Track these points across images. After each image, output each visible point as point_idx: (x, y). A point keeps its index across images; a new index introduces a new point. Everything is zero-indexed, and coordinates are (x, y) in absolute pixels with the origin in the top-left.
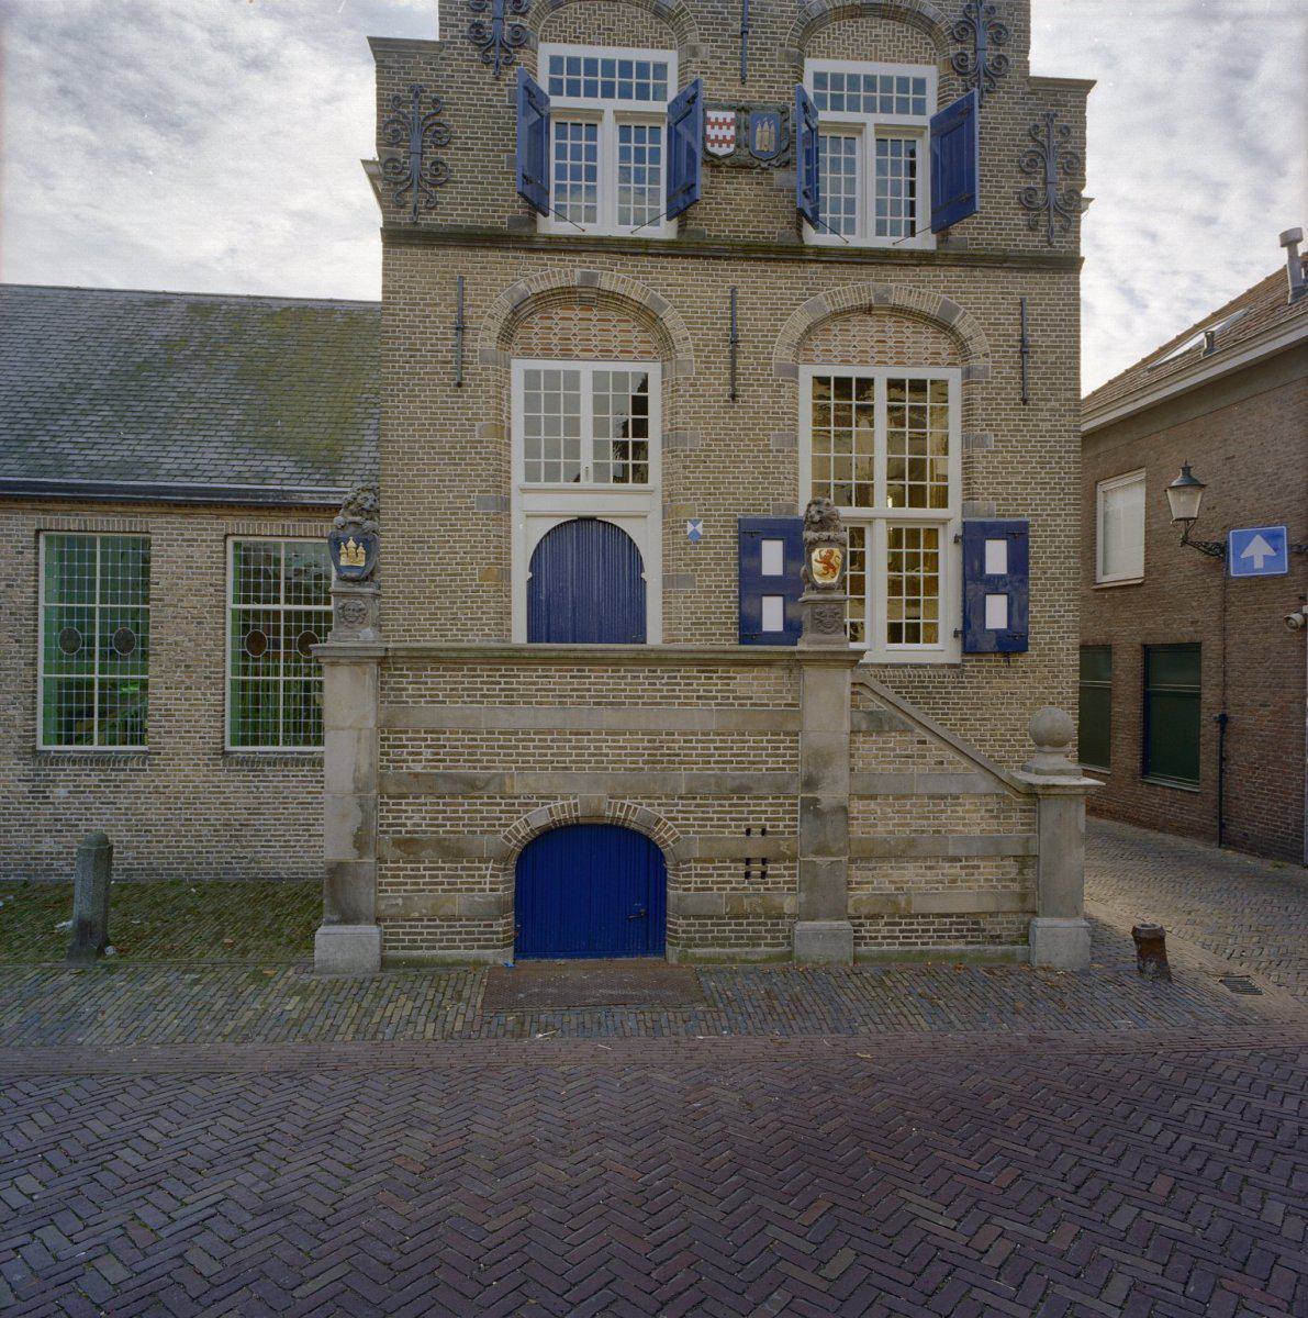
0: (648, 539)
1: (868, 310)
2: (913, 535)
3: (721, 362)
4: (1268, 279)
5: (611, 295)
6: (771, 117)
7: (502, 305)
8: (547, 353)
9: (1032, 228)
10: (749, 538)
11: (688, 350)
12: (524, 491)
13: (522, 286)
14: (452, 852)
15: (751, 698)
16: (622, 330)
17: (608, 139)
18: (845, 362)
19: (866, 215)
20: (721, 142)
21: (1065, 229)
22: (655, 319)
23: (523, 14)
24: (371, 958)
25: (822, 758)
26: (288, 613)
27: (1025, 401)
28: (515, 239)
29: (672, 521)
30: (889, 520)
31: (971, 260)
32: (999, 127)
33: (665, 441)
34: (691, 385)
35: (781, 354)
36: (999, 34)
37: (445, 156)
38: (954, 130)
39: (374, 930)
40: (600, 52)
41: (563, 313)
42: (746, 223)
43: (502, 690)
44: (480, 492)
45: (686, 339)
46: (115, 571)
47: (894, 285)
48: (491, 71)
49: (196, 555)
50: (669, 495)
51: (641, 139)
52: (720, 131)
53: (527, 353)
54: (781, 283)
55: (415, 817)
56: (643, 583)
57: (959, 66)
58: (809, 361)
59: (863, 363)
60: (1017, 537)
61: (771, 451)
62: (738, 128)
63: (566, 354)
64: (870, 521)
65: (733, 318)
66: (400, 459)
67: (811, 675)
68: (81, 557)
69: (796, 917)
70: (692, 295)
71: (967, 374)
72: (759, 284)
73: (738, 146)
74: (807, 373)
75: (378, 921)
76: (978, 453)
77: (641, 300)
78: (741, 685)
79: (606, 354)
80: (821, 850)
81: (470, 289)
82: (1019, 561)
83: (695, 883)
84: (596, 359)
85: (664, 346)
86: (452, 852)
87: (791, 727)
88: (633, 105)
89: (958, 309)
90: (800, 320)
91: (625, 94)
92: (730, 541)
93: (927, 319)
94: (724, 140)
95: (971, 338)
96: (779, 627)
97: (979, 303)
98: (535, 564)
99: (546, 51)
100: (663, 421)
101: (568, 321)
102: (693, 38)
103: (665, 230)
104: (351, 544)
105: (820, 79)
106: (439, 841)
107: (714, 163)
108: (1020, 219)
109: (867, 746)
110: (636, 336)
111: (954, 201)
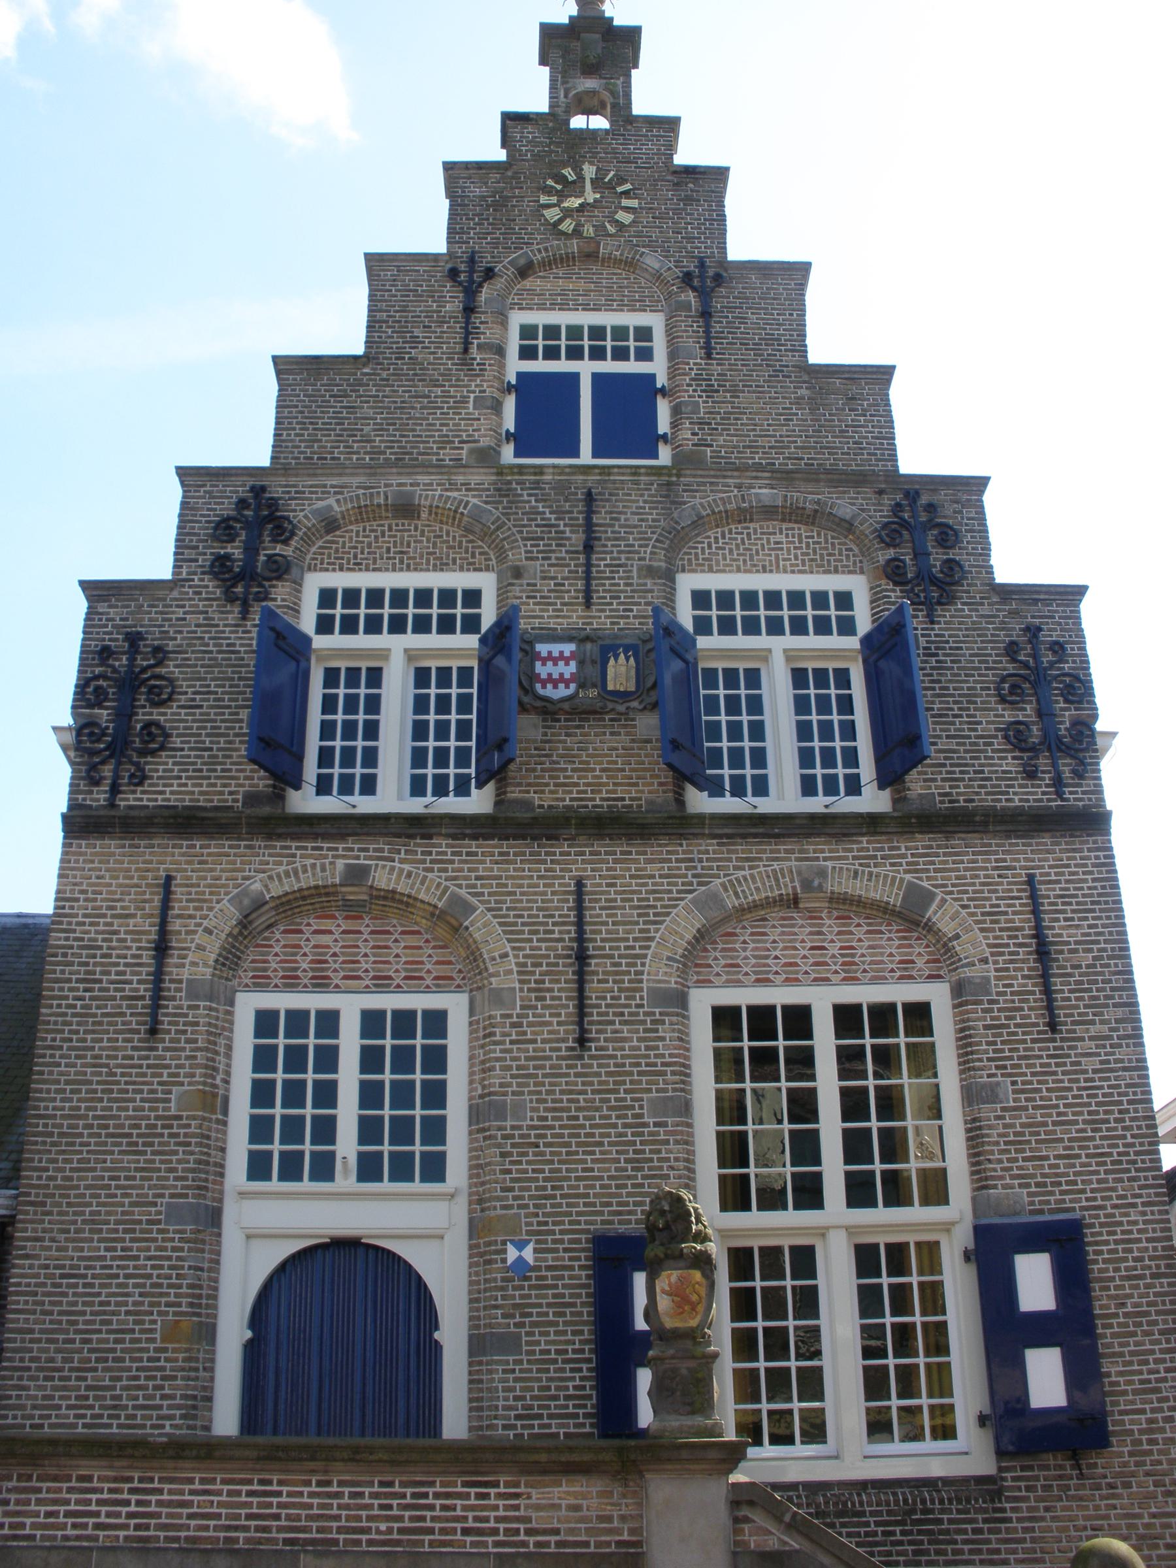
2: (898, 1253)
3: (562, 989)
5: (390, 896)
6: (627, 649)
7: (224, 915)
8: (291, 983)
11: (510, 972)
12: (243, 1195)
13: (257, 886)
15: (556, 1532)
18: (763, 981)
21: (1079, 775)
23: (286, 542)
27: (1053, 1026)
28: (270, 822)
29: (483, 1235)
30: (850, 1230)
32: (959, 640)
33: (476, 1114)
34: (513, 1025)
41: (316, 924)
43: (131, 1515)
44: (172, 1196)
45: (506, 955)
47: (829, 864)
48: (236, 610)
50: (478, 1201)
52: (557, 669)
53: (261, 983)
54: (650, 869)
56: (437, 1347)
57: (894, 572)
58: (705, 983)
59: (791, 981)
60: (1065, 1242)
61: (645, 1125)
62: (581, 663)
63: (321, 983)
64: (822, 1232)
65: (580, 923)
66: (54, 1144)
70: (513, 898)
71: (958, 989)
73: (582, 686)
74: (702, 1003)
76: (987, 1112)
77: (435, 901)
78: (538, 1508)
79: (382, 983)
81: (178, 892)
82: (1072, 1278)
84: (367, 990)
85: (470, 971)
89: (932, 896)
90: (684, 922)
92: (576, 1278)
93: (883, 910)
95: (957, 937)
97: (972, 887)
100: (471, 1082)
101: (326, 936)
105: (700, 599)
108: (1010, 764)
111: (899, 751)
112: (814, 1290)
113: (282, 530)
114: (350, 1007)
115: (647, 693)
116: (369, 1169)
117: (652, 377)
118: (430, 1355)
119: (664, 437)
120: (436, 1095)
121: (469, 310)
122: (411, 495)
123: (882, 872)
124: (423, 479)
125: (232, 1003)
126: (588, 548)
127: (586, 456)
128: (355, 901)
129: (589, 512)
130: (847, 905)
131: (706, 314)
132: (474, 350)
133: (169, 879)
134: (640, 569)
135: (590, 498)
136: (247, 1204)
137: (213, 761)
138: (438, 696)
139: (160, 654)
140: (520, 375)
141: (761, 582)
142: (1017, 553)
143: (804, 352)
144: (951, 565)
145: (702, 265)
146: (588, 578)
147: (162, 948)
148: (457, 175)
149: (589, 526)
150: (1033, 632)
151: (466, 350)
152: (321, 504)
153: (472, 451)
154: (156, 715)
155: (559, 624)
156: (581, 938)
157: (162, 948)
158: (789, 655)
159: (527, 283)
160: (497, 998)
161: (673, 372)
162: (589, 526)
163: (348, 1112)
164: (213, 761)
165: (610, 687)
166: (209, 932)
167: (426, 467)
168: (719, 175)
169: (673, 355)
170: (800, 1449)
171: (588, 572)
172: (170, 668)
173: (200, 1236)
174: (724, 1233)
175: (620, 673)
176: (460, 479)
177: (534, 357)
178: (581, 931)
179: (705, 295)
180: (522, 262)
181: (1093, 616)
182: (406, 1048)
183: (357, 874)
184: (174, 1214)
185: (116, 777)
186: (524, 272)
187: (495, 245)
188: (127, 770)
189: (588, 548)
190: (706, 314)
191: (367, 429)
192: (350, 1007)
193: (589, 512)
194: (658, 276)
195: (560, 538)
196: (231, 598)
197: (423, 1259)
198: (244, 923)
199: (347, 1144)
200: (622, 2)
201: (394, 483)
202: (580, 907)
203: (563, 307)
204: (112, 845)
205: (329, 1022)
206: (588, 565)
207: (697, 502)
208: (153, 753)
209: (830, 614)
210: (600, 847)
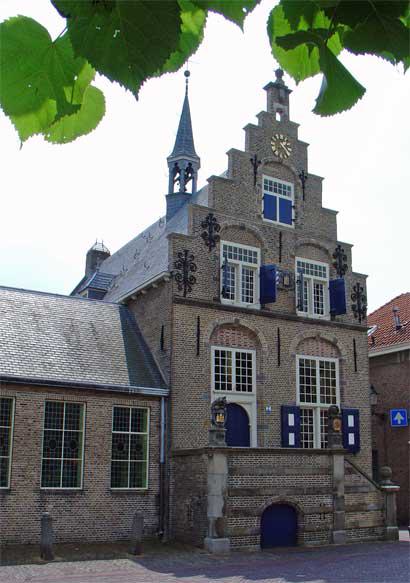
0: (252, 413)
1: (314, 338)
4: (317, 100)
7: (210, 327)
8: (222, 344)
9: (356, 317)
10: (285, 411)
14: (247, 513)
16: (245, 339)
22: (255, 336)
24: (227, 547)
25: (338, 482)
26: (132, 435)
31: (342, 326)
32: (347, 278)
33: (258, 377)
35: (292, 351)
36: (345, 258)
37: (196, 274)
38: (337, 290)
40: (248, 248)
46: (50, 415)
53: (216, 344)
57: (335, 265)
60: (356, 414)
63: (228, 345)
69: (334, 530)
70: (266, 329)
71: (340, 361)
72: (287, 328)
79: (239, 346)
80: (339, 509)
82: (356, 422)
83: (308, 521)
85: (258, 345)
86: (247, 513)
90: (296, 340)
91: (245, 260)
92: (278, 414)
93: (328, 342)
96: (319, 447)
99: (223, 242)
101: (228, 334)
109: (347, 478)
113: (217, 228)
114: (234, 351)
117: (291, 202)
118: (247, 428)
120: (250, 372)
123: (329, 334)
127: (264, 191)
129: (280, 238)
130: (323, 340)
142: (357, 266)
144: (346, 266)
147: (198, 335)
148: (249, 128)
150: (358, 284)
157: (198, 335)
158: (315, 280)
160: (264, 353)
161: (296, 203)
169: (296, 197)
173: (94, 468)
181: (368, 281)
182: (244, 361)
183: (237, 321)
186: (266, 164)
192: (234, 351)
193: (280, 238)
199: (234, 383)
209: (319, 271)
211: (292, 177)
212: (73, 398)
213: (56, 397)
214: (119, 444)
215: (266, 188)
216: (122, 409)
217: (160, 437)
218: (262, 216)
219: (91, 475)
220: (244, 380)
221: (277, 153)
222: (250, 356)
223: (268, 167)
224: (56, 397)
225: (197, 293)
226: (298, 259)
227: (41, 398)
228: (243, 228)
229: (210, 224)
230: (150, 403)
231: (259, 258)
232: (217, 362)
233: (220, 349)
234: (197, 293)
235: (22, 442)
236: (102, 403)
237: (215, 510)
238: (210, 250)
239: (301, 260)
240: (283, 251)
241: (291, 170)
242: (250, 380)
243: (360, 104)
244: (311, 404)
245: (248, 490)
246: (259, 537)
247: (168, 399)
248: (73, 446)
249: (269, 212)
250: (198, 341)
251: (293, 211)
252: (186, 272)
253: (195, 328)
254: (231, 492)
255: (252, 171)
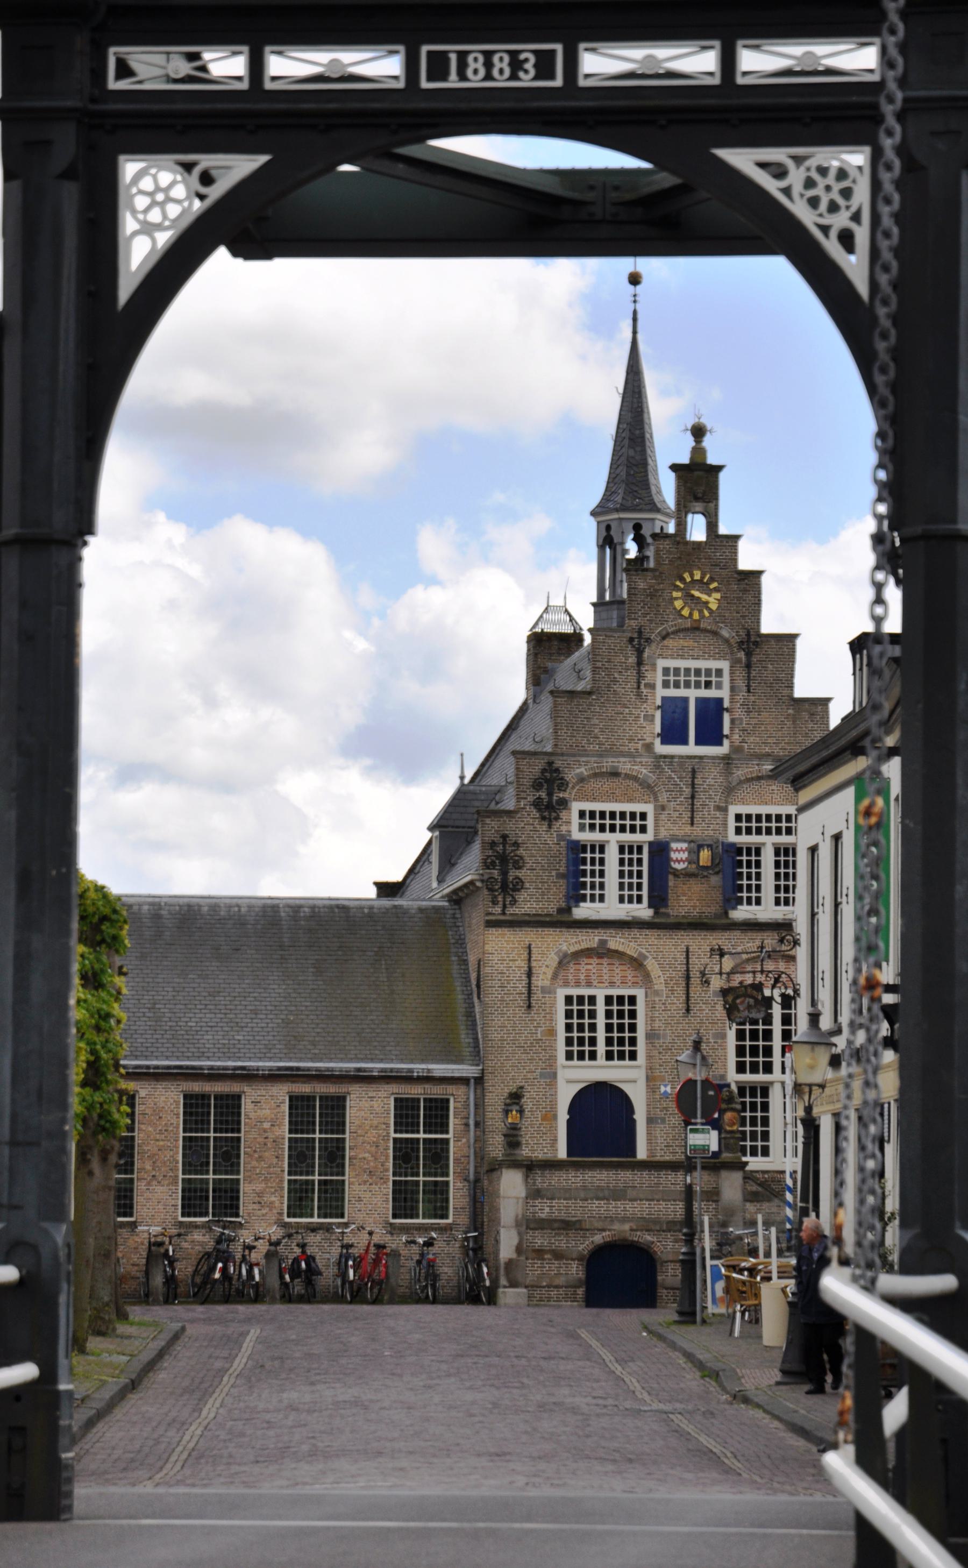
3: (681, 991)
5: (616, 951)
7: (553, 960)
8: (578, 984)
12: (564, 1067)
14: (558, 1255)
16: (619, 970)
17: (612, 856)
19: (768, 893)
20: (678, 861)
26: (424, 1140)
28: (562, 921)
29: (652, 1081)
37: (521, 874)
39: (524, 1290)
41: (586, 961)
42: (694, 907)
49: (376, 1106)
50: (650, 1069)
51: (631, 852)
52: (679, 855)
53: (566, 984)
55: (540, 1240)
56: (634, 1121)
62: (689, 853)
63: (589, 984)
64: (772, 1083)
65: (688, 963)
67: (724, 1174)
68: (308, 1107)
72: (701, 943)
73: (690, 863)
75: (526, 1287)
79: (612, 984)
81: (534, 950)
86: (558, 1255)
87: (715, 1198)
88: (628, 837)
94: (682, 860)
98: (570, 1111)
99: (576, 806)
101: (590, 966)
102: (663, 798)
103: (643, 911)
104: (514, 1112)
106: (553, 1250)
107: (676, 874)
110: (630, 974)
112: (768, 1103)
115: (715, 866)
116: (609, 1056)
119: (727, 737)
120: (633, 1028)
121: (640, 663)
122: (617, 767)
124: (622, 759)
125: (555, 993)
126: (693, 797)
128: (602, 952)
131: (748, 666)
132: (642, 686)
133: (530, 945)
134: (715, 806)
135: (694, 772)
136: (566, 1070)
137: (543, 894)
138: (756, 1111)
139: (516, 845)
140: (664, 699)
141: (764, 810)
143: (791, 686)
145: (748, 635)
146: (693, 811)
147: (529, 974)
149: (693, 785)
151: (639, 687)
152: (578, 771)
153: (643, 745)
154: (518, 873)
155: (680, 833)
156: (688, 970)
157: (529, 974)
159: (666, 642)
160: (657, 993)
161: (732, 700)
162: (693, 785)
163: (601, 1035)
164: (543, 894)
165: (701, 864)
166: (547, 966)
167: (622, 754)
168: (757, 574)
169: (733, 689)
170: (760, 1158)
171: (692, 808)
172: (521, 852)
174: (737, 1082)
175: (705, 855)
176: (638, 760)
177: (771, 1063)
178: (688, 968)
179: (749, 654)
180: (664, 633)
182: (622, 1008)
183: (603, 943)
184: (542, 1075)
185: (504, 901)
187: (650, 621)
188: (509, 899)
189: (693, 797)
190: (748, 666)
191: (596, 731)
193: (693, 778)
194: (727, 641)
195: (681, 791)
196: (543, 818)
197: (626, 1088)
198: (560, 963)
199: (601, 1048)
200: (707, 422)
201: (609, 763)
202: (687, 958)
203: (682, 657)
204: (506, 931)
205: (592, 1000)
206: (693, 804)
207: (740, 773)
208: (519, 890)
210: (695, 933)
211: (727, 649)
212: (331, 1089)
213: (305, 1089)
214: (405, 1154)
215: (666, 684)
216: (407, 1099)
217: (468, 1141)
218: (658, 741)
219: (360, 1199)
220: (621, 1041)
221: (686, 612)
222: (632, 1000)
223: (669, 642)
224: (305, 1089)
225: (527, 904)
226: (733, 810)
227: (281, 1093)
228: (615, 774)
229: (547, 781)
230: (451, 1089)
231: (650, 822)
232: (569, 1014)
233: (575, 992)
234: (527, 904)
235: (256, 1156)
236: (374, 1094)
237: (506, 1251)
238: (550, 826)
239: (744, 810)
240: (698, 804)
241: (722, 637)
242: (633, 1041)
243: (670, 464)
244: (761, 1077)
245: (563, 1221)
246: (581, 1291)
247: (480, 1081)
248: (334, 1156)
249: (673, 732)
250: (529, 984)
251: (726, 718)
252: (504, 873)
253: (524, 965)
254: (529, 1224)
255: (632, 660)
